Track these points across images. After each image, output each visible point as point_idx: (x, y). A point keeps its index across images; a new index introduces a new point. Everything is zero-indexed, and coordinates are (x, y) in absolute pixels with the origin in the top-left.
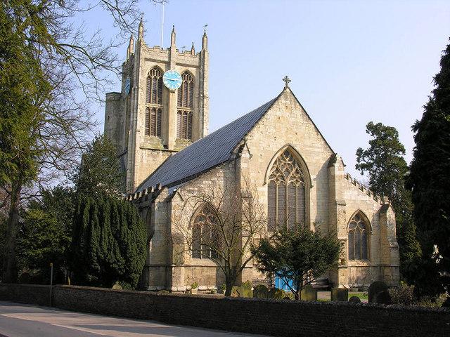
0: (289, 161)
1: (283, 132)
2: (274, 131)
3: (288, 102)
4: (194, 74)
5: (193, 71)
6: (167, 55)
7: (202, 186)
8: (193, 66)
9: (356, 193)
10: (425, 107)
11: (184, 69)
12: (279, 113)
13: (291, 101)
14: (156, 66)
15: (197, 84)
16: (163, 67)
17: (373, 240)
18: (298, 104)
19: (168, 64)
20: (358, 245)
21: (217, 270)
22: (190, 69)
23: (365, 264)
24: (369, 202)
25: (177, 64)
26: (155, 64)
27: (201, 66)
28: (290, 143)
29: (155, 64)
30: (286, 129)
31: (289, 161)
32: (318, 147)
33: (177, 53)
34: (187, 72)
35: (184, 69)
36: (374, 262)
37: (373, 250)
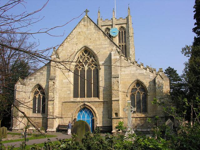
0: (87, 55)
1: (82, 40)
2: (76, 40)
3: (86, 23)
4: (125, 27)
5: (124, 26)
6: (111, 22)
7: (36, 76)
8: (124, 24)
9: (135, 68)
10: (194, 7)
11: (120, 26)
12: (79, 30)
13: (87, 22)
14: (107, 28)
15: (127, 32)
16: (110, 27)
17: (149, 98)
18: (92, 22)
19: (112, 25)
20: (139, 102)
21: (43, 119)
22: (123, 25)
23: (143, 116)
24: (146, 74)
25: (116, 25)
26: (106, 27)
27: (127, 23)
28: (86, 45)
29: (106, 27)
30: (84, 38)
31: (87, 55)
32: (105, 44)
33: (116, 20)
34: (122, 27)
35: (120, 26)
36: (150, 114)
37: (149, 106)
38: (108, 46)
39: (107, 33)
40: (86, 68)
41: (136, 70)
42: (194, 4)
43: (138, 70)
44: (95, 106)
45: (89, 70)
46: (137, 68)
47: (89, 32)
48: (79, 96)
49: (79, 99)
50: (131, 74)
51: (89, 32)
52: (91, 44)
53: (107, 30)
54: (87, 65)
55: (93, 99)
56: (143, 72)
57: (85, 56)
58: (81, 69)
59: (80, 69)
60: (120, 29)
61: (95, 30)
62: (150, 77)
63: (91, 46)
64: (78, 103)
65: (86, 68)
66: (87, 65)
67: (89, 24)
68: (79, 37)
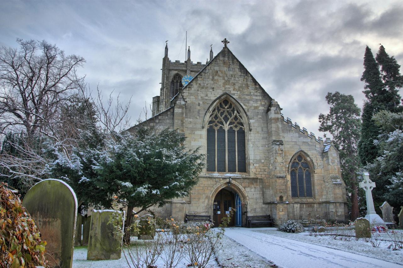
3: (226, 59)
12: (217, 68)
29: (176, 72)
32: (257, 96)
38: (261, 98)
39: (177, 81)
40: (226, 127)
41: (299, 137)
42: (364, 56)
43: (302, 138)
44: (243, 185)
45: (231, 131)
46: (300, 134)
47: (231, 73)
48: (216, 169)
49: (216, 174)
50: (293, 142)
51: (231, 73)
52: (236, 92)
53: (176, 77)
54: (228, 123)
55: (237, 175)
56: (307, 141)
57: (224, 108)
58: (218, 127)
59: (216, 129)
60: (174, 77)
61: (241, 72)
62: (316, 148)
63: (236, 94)
64: (216, 179)
65: (226, 127)
66: (228, 123)
67: (231, 62)
68: (216, 78)
